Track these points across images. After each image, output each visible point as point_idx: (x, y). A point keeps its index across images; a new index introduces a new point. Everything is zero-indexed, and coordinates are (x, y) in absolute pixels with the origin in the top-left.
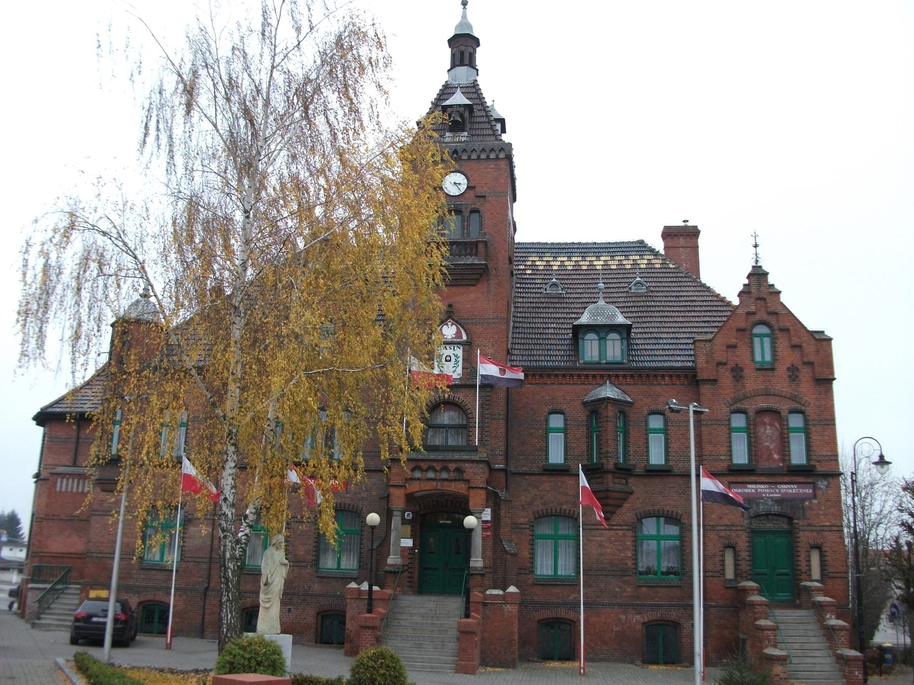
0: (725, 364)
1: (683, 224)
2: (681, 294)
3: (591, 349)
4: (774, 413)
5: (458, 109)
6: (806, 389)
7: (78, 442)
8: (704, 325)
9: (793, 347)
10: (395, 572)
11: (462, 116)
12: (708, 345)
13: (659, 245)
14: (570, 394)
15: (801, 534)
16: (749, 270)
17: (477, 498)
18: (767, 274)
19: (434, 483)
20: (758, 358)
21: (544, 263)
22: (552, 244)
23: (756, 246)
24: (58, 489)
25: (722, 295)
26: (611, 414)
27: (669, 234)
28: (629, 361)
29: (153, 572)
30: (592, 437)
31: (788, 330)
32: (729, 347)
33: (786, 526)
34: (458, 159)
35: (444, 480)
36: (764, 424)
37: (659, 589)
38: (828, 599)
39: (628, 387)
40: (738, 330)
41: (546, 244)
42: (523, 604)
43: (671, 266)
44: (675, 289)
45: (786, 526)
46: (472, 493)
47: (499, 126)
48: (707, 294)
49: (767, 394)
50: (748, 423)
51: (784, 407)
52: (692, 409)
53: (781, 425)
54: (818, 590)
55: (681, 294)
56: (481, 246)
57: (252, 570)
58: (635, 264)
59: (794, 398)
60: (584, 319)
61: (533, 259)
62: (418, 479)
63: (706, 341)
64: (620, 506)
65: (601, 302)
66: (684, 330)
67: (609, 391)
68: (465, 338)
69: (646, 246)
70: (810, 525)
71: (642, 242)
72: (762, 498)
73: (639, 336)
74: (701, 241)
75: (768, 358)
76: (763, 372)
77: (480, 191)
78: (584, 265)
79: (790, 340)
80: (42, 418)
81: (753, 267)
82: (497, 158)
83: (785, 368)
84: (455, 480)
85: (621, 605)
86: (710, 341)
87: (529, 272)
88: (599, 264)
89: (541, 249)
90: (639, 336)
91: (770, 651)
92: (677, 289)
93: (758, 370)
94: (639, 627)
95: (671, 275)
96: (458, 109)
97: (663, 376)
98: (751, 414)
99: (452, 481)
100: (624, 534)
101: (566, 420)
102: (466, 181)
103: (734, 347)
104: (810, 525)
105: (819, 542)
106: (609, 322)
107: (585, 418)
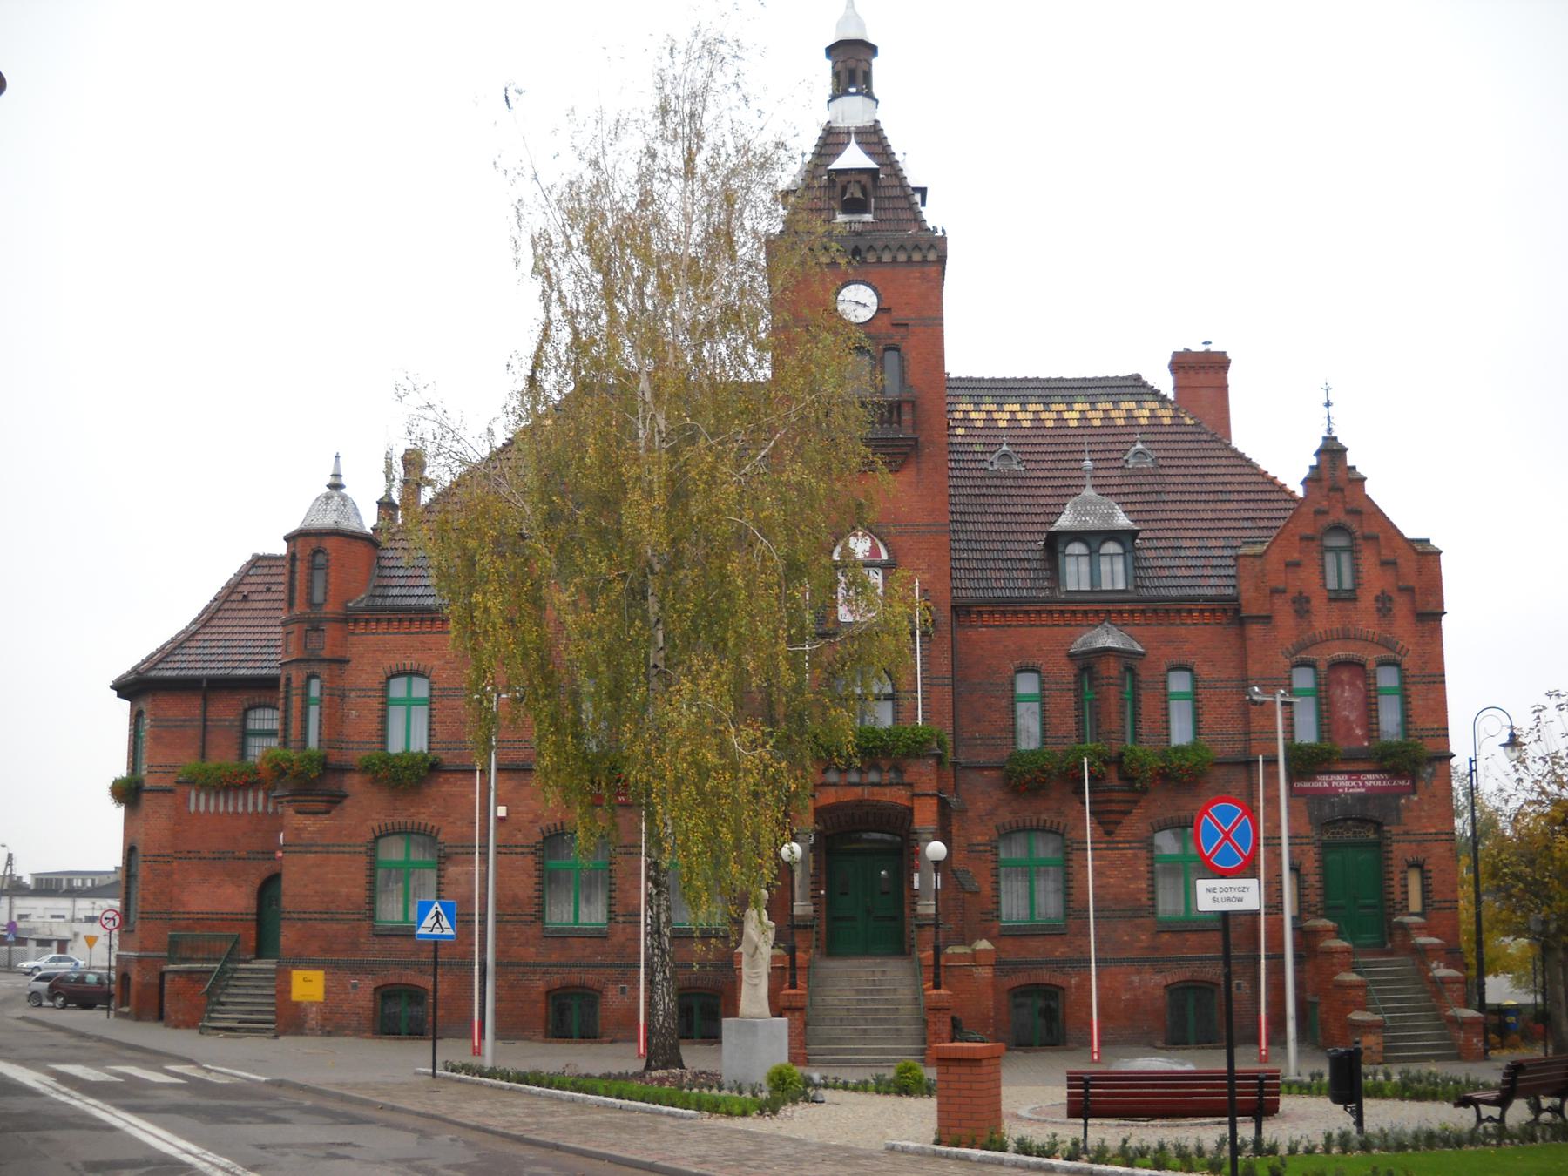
0: (1284, 592)
1: (1202, 348)
2: (1207, 471)
3: (1076, 573)
4: (1356, 666)
5: (858, 178)
6: (1403, 628)
7: (205, 726)
8: (1245, 524)
9: (1384, 563)
10: (805, 927)
11: (864, 189)
12: (1258, 562)
13: (1164, 383)
14: (1040, 639)
15: (1395, 846)
16: (1318, 443)
17: (925, 815)
18: (1346, 450)
19: (859, 790)
20: (1332, 584)
21: (984, 416)
22: (993, 380)
23: (1328, 405)
24: (192, 808)
25: (1272, 474)
26: (1113, 673)
27: (1183, 364)
28: (1137, 587)
29: (395, 940)
30: (1083, 708)
31: (1375, 538)
32: (1287, 565)
33: (1372, 836)
34: (860, 258)
35: (874, 785)
36: (1341, 683)
37: (1188, 936)
38: (1436, 941)
39: (1136, 629)
40: (1302, 539)
41: (982, 380)
42: (1000, 965)
43: (1188, 421)
44: (1196, 462)
45: (1372, 836)
46: (917, 803)
47: (918, 197)
48: (1247, 470)
49: (1346, 637)
50: (1318, 684)
51: (1370, 656)
52: (1279, 699)
53: (1366, 684)
54: (1420, 928)
55: (1207, 471)
56: (906, 409)
57: (557, 931)
58: (1130, 417)
59: (1385, 644)
60: (1065, 522)
61: (965, 407)
62: (834, 785)
63: (1255, 556)
64: (1127, 813)
65: (1089, 492)
66: (1216, 533)
67: (1108, 638)
68: (884, 556)
69: (1145, 385)
70: (1407, 833)
71: (1137, 378)
72: (1338, 795)
73: (1148, 544)
74: (1233, 376)
75: (1347, 584)
76: (1340, 604)
77: (897, 315)
78: (1049, 419)
79: (1379, 553)
80: (128, 687)
81: (1325, 438)
82: (924, 261)
83: (1372, 598)
84: (891, 784)
85: (1132, 961)
86: (1260, 556)
87: (961, 431)
88: (1072, 417)
89: (978, 389)
90: (1148, 544)
91: (1357, 1016)
92: (1200, 462)
93: (1331, 600)
94: (1160, 992)
95: (1190, 437)
96: (858, 178)
97: (1190, 611)
98: (1323, 668)
99: (886, 785)
100: (1135, 855)
101: (1042, 682)
102: (875, 299)
103: (1297, 565)
104: (1407, 833)
105: (1421, 857)
106: (1106, 527)
107: (1072, 679)
